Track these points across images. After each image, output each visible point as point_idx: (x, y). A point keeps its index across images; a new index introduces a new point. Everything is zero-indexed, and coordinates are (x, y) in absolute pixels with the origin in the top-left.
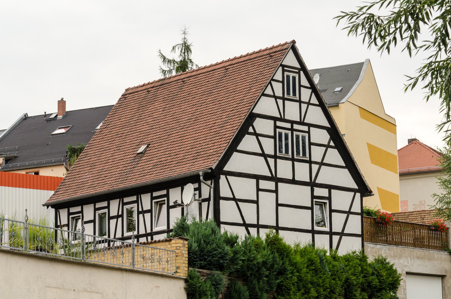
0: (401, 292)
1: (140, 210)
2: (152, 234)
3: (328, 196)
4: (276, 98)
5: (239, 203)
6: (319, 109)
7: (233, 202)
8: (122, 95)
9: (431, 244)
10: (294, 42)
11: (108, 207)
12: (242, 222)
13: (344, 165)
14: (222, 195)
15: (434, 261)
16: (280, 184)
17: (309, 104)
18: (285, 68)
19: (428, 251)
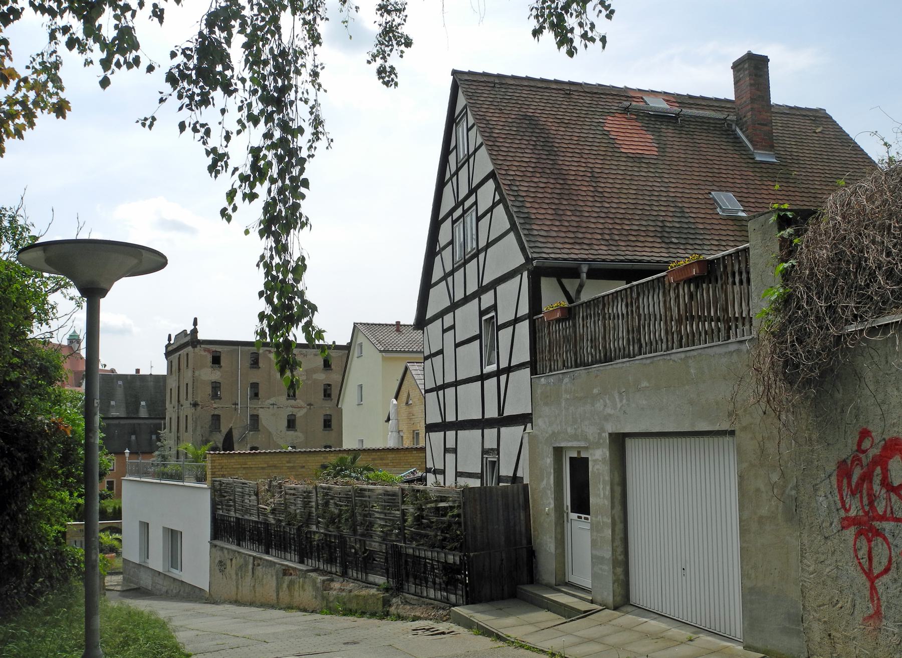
0: (599, 489)
15: (687, 387)
19: (668, 358)
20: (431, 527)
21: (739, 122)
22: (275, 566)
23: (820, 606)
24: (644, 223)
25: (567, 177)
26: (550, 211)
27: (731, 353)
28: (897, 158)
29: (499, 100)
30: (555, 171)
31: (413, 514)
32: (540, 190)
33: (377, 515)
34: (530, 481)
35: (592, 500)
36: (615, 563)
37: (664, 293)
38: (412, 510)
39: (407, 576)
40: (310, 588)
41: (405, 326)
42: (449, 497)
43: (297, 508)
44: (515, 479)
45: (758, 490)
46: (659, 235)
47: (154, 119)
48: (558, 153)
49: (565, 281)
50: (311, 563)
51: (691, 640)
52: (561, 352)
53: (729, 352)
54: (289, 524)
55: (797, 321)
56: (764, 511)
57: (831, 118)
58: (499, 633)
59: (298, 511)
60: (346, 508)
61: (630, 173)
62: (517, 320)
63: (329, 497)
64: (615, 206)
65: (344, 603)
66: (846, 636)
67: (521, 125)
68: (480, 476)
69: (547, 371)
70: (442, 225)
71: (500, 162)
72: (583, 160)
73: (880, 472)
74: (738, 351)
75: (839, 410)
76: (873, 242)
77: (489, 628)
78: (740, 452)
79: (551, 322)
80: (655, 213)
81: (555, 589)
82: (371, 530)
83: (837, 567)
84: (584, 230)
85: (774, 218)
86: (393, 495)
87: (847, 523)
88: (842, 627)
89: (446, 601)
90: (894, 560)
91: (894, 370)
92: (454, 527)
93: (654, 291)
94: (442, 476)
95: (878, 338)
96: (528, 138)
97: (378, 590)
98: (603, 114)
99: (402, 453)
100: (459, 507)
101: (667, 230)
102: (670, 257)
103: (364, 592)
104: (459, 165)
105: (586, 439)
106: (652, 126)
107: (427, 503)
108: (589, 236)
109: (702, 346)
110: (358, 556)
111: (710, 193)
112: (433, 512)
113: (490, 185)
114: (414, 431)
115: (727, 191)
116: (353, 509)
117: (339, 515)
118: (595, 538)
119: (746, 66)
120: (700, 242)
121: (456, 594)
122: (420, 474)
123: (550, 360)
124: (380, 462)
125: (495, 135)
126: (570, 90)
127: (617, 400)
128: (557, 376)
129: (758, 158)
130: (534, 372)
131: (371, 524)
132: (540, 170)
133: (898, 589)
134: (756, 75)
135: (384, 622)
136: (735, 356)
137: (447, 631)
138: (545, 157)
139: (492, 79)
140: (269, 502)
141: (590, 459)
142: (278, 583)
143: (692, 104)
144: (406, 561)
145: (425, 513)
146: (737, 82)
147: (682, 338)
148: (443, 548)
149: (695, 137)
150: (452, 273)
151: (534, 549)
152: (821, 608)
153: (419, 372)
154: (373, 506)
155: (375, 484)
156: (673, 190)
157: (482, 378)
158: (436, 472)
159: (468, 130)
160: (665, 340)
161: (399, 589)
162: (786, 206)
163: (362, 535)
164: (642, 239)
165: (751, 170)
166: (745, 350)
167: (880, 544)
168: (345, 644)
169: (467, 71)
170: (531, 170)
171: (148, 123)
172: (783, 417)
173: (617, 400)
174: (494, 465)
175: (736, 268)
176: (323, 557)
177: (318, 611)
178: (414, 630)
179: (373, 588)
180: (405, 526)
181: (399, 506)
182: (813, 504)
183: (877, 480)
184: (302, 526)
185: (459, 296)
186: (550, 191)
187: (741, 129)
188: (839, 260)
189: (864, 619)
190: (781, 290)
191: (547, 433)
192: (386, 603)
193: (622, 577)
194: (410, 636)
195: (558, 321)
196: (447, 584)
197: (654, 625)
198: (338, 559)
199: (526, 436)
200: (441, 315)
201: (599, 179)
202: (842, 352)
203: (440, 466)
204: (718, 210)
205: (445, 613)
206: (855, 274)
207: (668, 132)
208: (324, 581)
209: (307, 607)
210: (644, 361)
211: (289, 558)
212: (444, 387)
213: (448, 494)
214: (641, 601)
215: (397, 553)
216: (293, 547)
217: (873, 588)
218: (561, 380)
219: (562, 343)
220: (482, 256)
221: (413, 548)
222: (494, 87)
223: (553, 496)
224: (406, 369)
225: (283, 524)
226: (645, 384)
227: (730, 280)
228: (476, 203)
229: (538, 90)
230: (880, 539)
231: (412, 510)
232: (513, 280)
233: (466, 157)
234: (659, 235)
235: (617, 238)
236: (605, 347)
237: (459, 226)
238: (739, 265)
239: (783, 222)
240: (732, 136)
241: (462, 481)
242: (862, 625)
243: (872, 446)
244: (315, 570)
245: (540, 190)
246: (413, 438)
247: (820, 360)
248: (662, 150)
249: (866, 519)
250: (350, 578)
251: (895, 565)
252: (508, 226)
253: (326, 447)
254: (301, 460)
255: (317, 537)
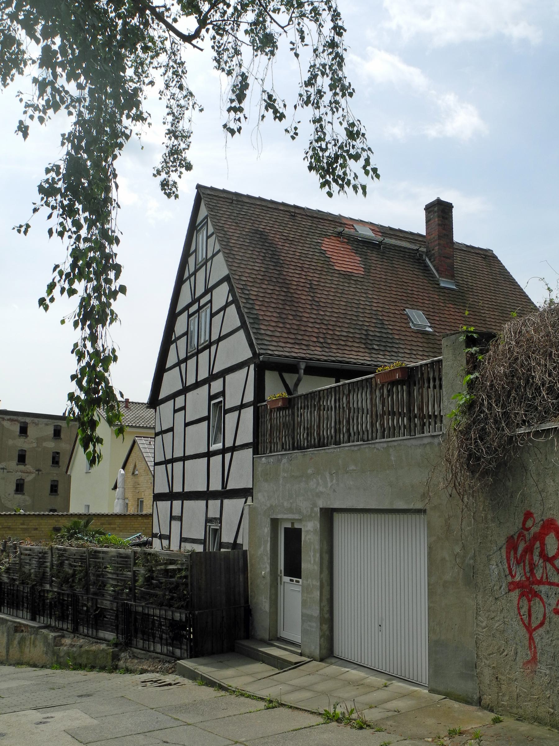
0: (310, 556)
9: (403, 420)
15: (388, 472)
19: (373, 446)
20: (159, 588)
21: (428, 253)
22: (7, 623)
23: (490, 655)
24: (352, 331)
25: (290, 286)
26: (275, 315)
27: (425, 445)
28: (556, 301)
29: (236, 215)
30: (280, 281)
31: (144, 575)
32: (267, 296)
33: (110, 576)
34: (249, 547)
35: (304, 566)
36: (322, 620)
37: (371, 392)
38: (143, 572)
39: (136, 631)
40: (42, 644)
41: (133, 403)
42: (177, 560)
43: (31, 568)
44: (235, 545)
45: (443, 560)
46: (363, 341)
47: (28, 226)
48: (283, 265)
49: (285, 375)
50: (43, 620)
51: (386, 686)
52: (281, 436)
53: (424, 444)
54: (23, 583)
55: (480, 423)
56: (448, 577)
57: (497, 258)
58: (222, 684)
59: (32, 571)
60: (81, 568)
61: (341, 288)
62: (242, 406)
63: (65, 558)
64: (328, 314)
65: (75, 658)
66: (510, 679)
67: (253, 238)
68: (203, 542)
69: (268, 452)
70: (178, 318)
71: (235, 269)
72: (304, 273)
73: (539, 546)
74: (431, 444)
75: (509, 496)
76: (539, 364)
77: (212, 679)
78: (430, 527)
79: (273, 410)
80: (361, 323)
81: (269, 644)
82: (104, 590)
83: (504, 623)
84: (302, 333)
85: (462, 338)
86: (126, 557)
87: (512, 586)
88: (507, 671)
89: (171, 655)
90: (547, 615)
91: (551, 465)
92: (181, 588)
93: (363, 389)
94: (167, 541)
95: (541, 440)
96: (259, 250)
97: (108, 645)
98: (320, 235)
99: (129, 518)
100: (186, 569)
101: (370, 338)
102: (372, 360)
103: (94, 648)
104: (197, 267)
105: (300, 512)
106: (360, 250)
107: (157, 566)
108: (307, 338)
109: (401, 438)
110: (89, 613)
111: (404, 310)
112: (162, 574)
113: (225, 287)
114: (138, 499)
115: (418, 309)
116: (87, 569)
117: (74, 575)
118: (305, 598)
119: (436, 209)
120: (396, 350)
121: (181, 649)
122: (145, 539)
123: (270, 442)
124: (109, 526)
125: (232, 245)
126: (295, 213)
127: (328, 480)
128: (276, 456)
129: (442, 285)
130: (256, 452)
131: (104, 585)
132: (268, 279)
133: (550, 639)
134: (443, 217)
135: (113, 675)
136: (428, 447)
137: (173, 683)
138: (272, 267)
139: (230, 196)
140: (3, 561)
141: (303, 530)
142: (8, 640)
143: (392, 235)
144: (136, 619)
145: (155, 575)
146: (428, 221)
147: (384, 430)
148: (171, 606)
149: (394, 262)
150: (185, 360)
151: (251, 608)
152: (491, 656)
153: (146, 446)
154: (106, 568)
155: (108, 547)
156: (375, 305)
157: (209, 455)
158: (161, 537)
159: (208, 237)
160: (370, 432)
161: (127, 645)
162: (472, 329)
163: (95, 594)
164: (350, 344)
165: (436, 293)
166: (436, 444)
167: (537, 603)
168: (79, 696)
169: (209, 186)
170: (260, 277)
171: (23, 229)
172: (466, 499)
173: (328, 480)
174: (217, 533)
175: (431, 376)
176: (55, 614)
177: (48, 666)
178: (143, 682)
179: (103, 643)
180: (135, 586)
181: (130, 568)
182: (487, 572)
183: (536, 552)
184: (35, 585)
185: (191, 381)
186: (275, 297)
187: (430, 260)
188: (512, 376)
189: (524, 664)
190: (468, 397)
191: (266, 506)
192: (116, 657)
193: (327, 633)
194: (140, 688)
195: (279, 409)
196: (173, 639)
197: (355, 674)
198: (70, 616)
199: (247, 509)
200: (173, 396)
201: (316, 291)
202: (513, 450)
203: (165, 532)
204: (411, 324)
205: (170, 666)
206: (525, 387)
207: (373, 256)
208: (55, 638)
209: (36, 662)
210: (353, 448)
211: (21, 615)
212: (173, 461)
213: (177, 557)
214: (343, 653)
215: (127, 611)
216: (26, 605)
217: (531, 639)
218: (280, 461)
219: (282, 428)
220: (213, 348)
221: (143, 607)
222: (232, 203)
223: (269, 561)
224: (134, 442)
225: (17, 583)
226: (352, 467)
227: (426, 385)
228: (210, 301)
229: (269, 209)
230: (537, 600)
231: (143, 572)
232: (241, 371)
233: (204, 261)
234: (363, 341)
235: (329, 341)
236: (319, 434)
237: (194, 319)
238: (434, 373)
239: (470, 341)
240: (423, 265)
241: (188, 547)
242: (522, 668)
243: (533, 526)
244: (47, 627)
245: (267, 296)
246: (138, 505)
247: (496, 455)
248: (368, 271)
249: (527, 583)
250: (80, 634)
251: (548, 619)
252: (239, 324)
253: (51, 510)
254: (34, 523)
255: (50, 595)
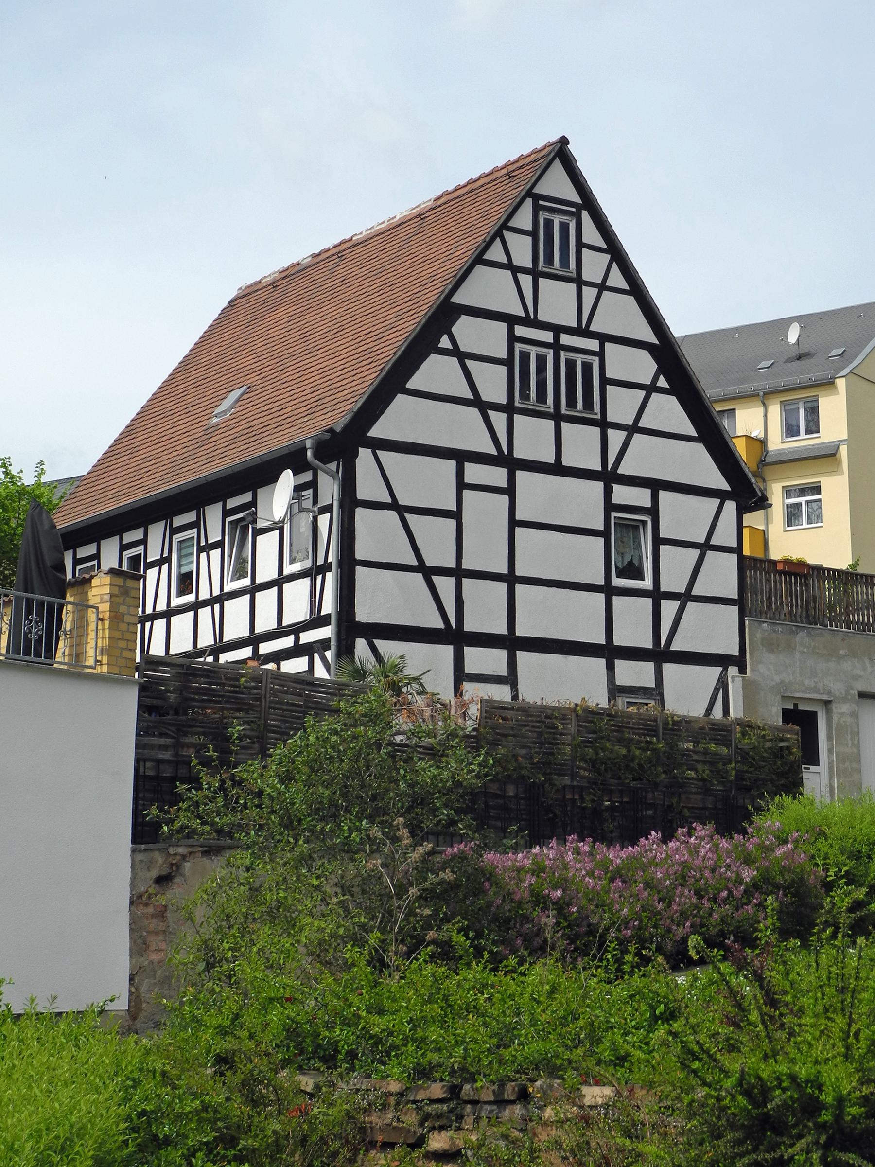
1: (203, 543)
2: (223, 597)
3: (650, 506)
4: (515, 270)
5: (407, 516)
6: (631, 300)
7: (393, 515)
8: (229, 303)
10: (564, 141)
11: (144, 542)
12: (414, 562)
13: (692, 432)
14: (361, 495)
16: (520, 475)
17: (602, 287)
18: (541, 202)
